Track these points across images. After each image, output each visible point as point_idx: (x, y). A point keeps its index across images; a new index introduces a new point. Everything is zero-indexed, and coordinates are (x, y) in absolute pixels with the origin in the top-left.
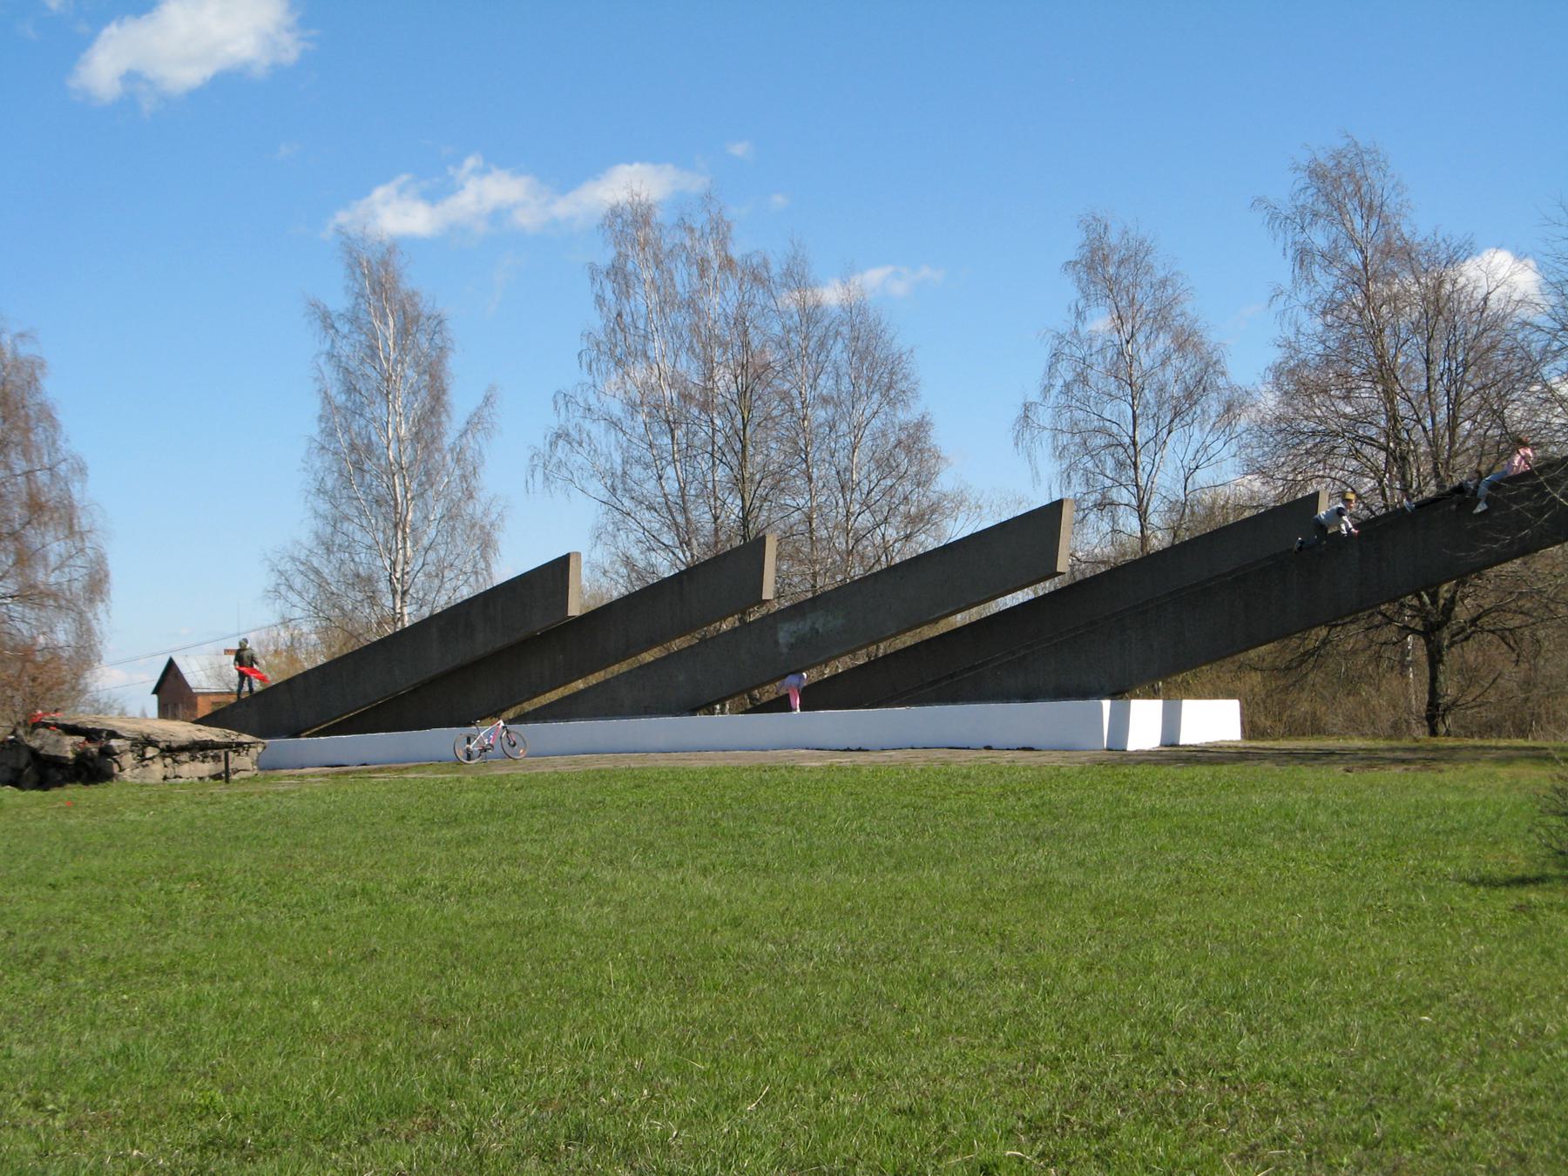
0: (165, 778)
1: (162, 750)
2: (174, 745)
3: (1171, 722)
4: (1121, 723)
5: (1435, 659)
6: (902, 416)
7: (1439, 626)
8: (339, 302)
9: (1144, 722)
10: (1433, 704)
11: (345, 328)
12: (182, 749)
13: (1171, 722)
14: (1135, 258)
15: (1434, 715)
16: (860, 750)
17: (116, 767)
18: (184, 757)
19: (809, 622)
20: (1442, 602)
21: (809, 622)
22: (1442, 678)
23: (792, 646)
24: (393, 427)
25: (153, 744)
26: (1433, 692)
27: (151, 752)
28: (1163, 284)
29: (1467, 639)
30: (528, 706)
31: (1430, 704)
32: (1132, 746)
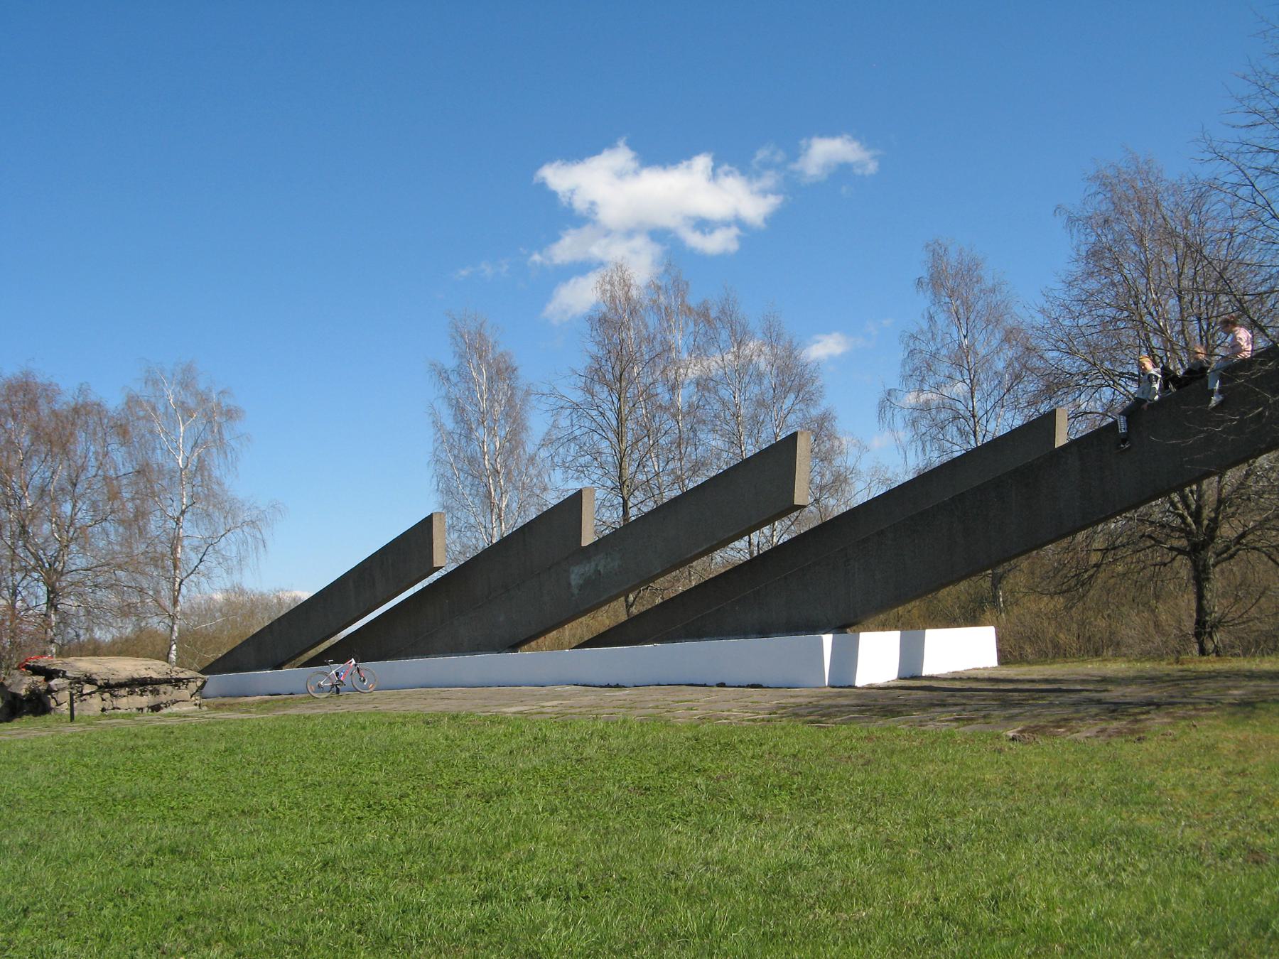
0: (103, 710)
1: (100, 687)
2: (112, 682)
3: (911, 654)
4: (846, 659)
5: (1200, 577)
6: (815, 412)
7: (1204, 546)
8: (450, 363)
9: (877, 657)
10: (1200, 623)
11: (454, 378)
12: (120, 685)
13: (911, 654)
14: (968, 273)
15: (1203, 628)
16: (617, 686)
17: (53, 701)
18: (123, 692)
19: (593, 564)
20: (1206, 522)
21: (593, 564)
22: (1208, 595)
23: (581, 588)
24: (489, 442)
25: (90, 681)
26: (1201, 610)
27: (88, 689)
28: (993, 290)
29: (1232, 557)
30: (313, 653)
31: (1198, 622)
32: (861, 680)
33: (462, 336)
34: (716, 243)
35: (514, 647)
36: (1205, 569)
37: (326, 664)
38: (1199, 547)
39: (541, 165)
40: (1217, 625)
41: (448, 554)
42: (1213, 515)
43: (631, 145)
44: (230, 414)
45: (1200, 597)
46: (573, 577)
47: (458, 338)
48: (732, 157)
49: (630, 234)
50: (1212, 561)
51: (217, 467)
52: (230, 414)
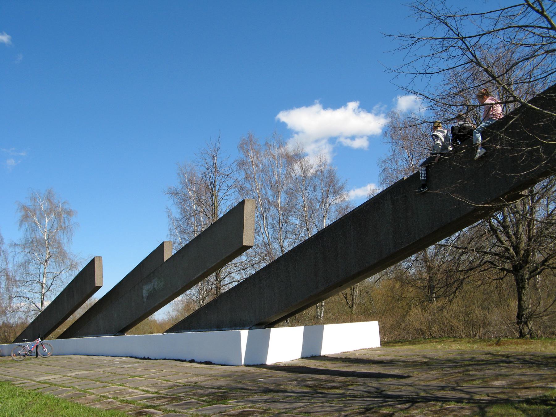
3: (312, 342)
4: (259, 347)
5: (520, 286)
9: (285, 344)
10: (519, 316)
15: (522, 318)
20: (522, 252)
22: (524, 298)
23: (148, 298)
26: (520, 308)
33: (184, 174)
34: (358, 144)
35: (122, 332)
36: (523, 281)
37: (24, 341)
38: (519, 268)
39: (277, 113)
40: (530, 316)
41: (109, 280)
42: (526, 248)
43: (320, 103)
44: (69, 213)
45: (520, 299)
46: (144, 291)
47: (182, 176)
48: (366, 106)
49: (317, 141)
50: (527, 276)
51: (62, 237)
52: (69, 213)
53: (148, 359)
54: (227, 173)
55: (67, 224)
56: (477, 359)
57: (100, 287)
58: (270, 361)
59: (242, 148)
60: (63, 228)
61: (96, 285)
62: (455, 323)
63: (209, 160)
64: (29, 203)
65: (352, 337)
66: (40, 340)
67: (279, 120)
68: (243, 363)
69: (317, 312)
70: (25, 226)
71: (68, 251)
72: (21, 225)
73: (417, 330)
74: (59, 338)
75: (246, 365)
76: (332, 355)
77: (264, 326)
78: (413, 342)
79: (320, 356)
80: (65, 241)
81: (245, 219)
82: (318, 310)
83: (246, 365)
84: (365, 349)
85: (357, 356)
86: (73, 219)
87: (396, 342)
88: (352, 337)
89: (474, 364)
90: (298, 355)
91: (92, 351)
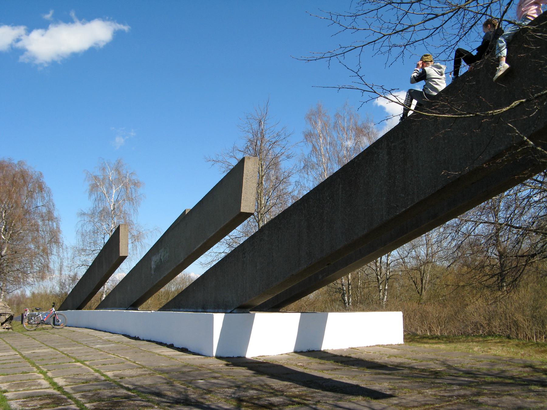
4: (240, 334)
9: (273, 335)
23: (155, 270)
35: (134, 306)
44: (136, 184)
46: (153, 263)
51: (126, 207)
52: (136, 184)
53: (136, 339)
54: (274, 140)
55: (134, 196)
56: (507, 374)
57: (125, 257)
58: (251, 353)
59: (310, 119)
60: (130, 200)
61: (121, 255)
62: (519, 317)
63: (255, 126)
64: (99, 173)
65: (365, 330)
66: (54, 310)
67: (377, 105)
68: (214, 354)
69: (380, 296)
70: (93, 197)
71: (135, 222)
72: (90, 195)
73: (476, 324)
74: (166, 307)
75: (218, 357)
76: (335, 351)
77: (248, 310)
78: (449, 339)
79: (320, 351)
80: (132, 211)
81: (244, 181)
82: (381, 293)
83: (218, 357)
84: (383, 346)
85: (363, 356)
86: (140, 191)
87: (423, 339)
88: (365, 330)
89: (492, 383)
90: (291, 348)
91: (98, 325)
